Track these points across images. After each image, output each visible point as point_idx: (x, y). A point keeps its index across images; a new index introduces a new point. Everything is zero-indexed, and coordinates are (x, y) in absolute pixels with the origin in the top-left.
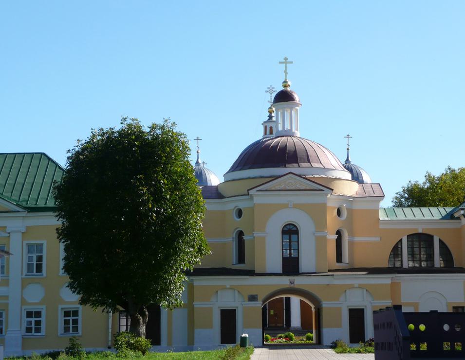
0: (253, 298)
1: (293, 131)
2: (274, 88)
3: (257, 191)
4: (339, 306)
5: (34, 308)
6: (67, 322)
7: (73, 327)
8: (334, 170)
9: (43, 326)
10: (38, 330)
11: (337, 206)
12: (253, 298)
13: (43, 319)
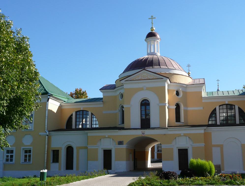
0: (121, 143)
1: (155, 52)
2: (190, 65)
3: (125, 81)
5: (27, 148)
6: (26, 156)
7: (28, 159)
9: (14, 157)
10: (11, 160)
11: (176, 89)
12: (121, 143)
13: (14, 154)
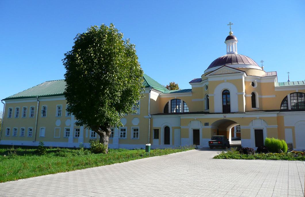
0: (207, 124)
4: (249, 128)
5: (136, 127)
6: (134, 134)
8: (250, 65)
9: (126, 135)
10: (124, 136)
12: (207, 124)
13: (126, 132)
